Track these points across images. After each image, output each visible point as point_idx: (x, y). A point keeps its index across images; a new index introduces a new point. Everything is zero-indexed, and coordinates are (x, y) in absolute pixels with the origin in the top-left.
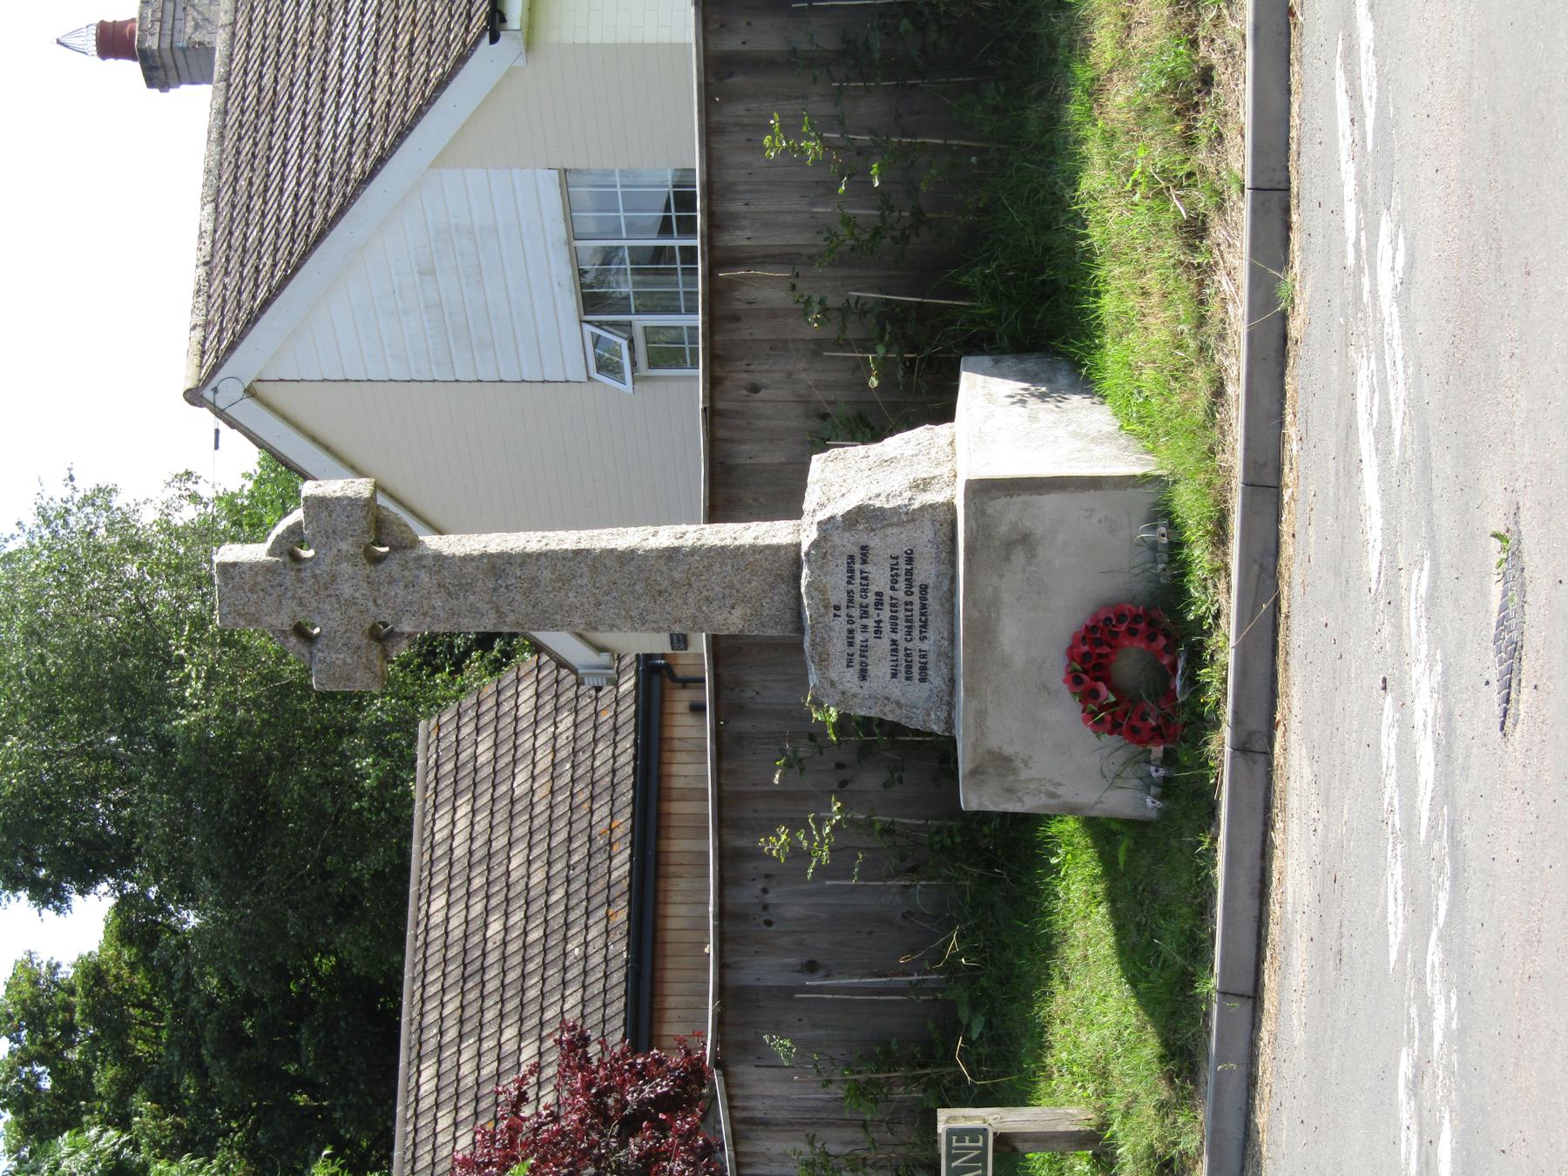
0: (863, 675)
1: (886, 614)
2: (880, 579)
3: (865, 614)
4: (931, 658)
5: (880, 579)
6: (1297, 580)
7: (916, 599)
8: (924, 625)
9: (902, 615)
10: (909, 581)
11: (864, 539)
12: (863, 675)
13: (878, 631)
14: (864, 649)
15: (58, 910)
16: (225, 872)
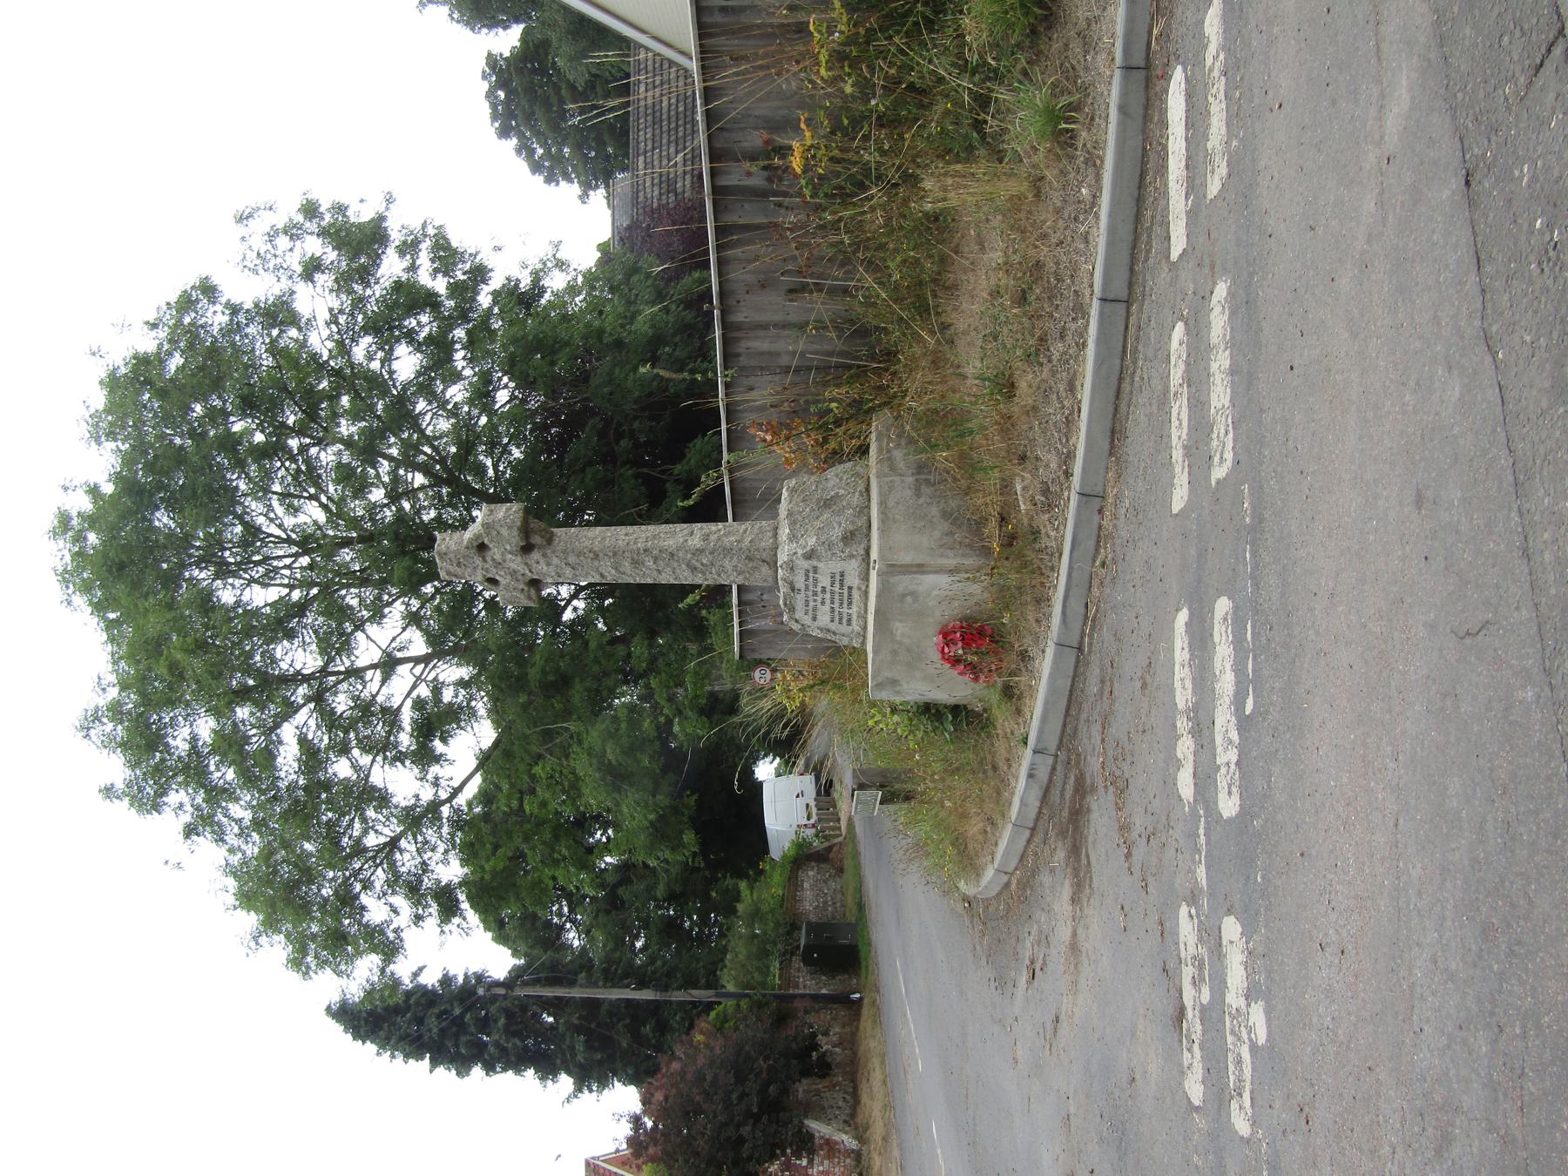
0: (814, 619)
1: (828, 596)
2: (824, 581)
3: (815, 594)
4: (854, 617)
5: (824, 581)
6: (871, 891)
7: (846, 592)
8: (850, 603)
9: (837, 597)
10: (842, 585)
11: (815, 563)
12: (814, 619)
13: (823, 603)
14: (815, 609)
15: (459, 1074)
16: (502, 1021)
